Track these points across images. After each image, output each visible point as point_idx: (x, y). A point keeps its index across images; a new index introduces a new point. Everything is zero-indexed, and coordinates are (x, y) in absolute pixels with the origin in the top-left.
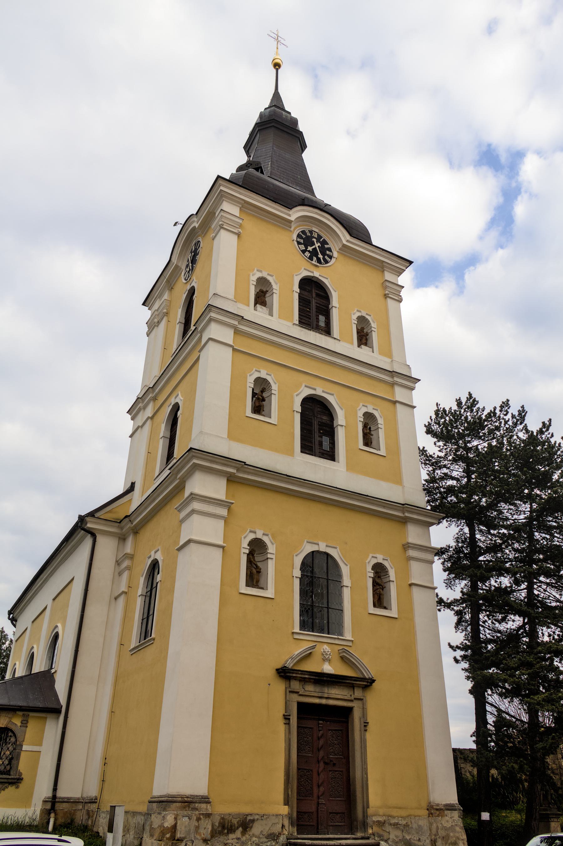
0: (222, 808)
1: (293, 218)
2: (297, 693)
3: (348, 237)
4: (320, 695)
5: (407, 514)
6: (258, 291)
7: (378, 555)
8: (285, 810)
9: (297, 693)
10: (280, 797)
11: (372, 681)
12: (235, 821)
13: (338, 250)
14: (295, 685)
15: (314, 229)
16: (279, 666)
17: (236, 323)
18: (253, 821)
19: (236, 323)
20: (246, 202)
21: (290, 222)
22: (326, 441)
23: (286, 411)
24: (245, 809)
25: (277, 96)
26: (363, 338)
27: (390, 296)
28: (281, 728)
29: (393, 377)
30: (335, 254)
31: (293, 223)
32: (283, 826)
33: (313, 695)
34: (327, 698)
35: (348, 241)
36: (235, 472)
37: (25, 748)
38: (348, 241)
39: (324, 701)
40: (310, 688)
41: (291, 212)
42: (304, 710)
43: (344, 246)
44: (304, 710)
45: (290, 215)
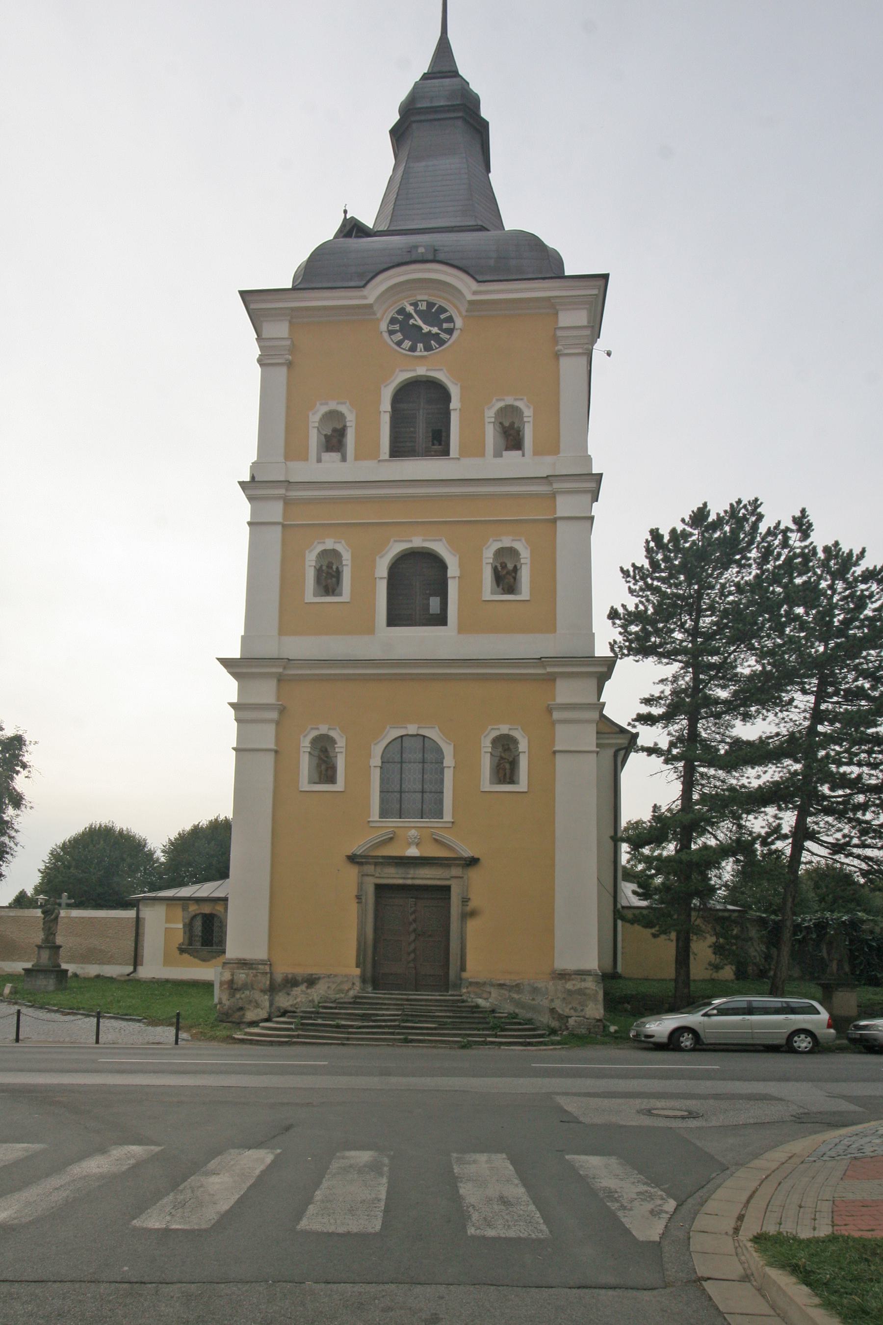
0: (282, 970)
1: (370, 300)
2: (373, 875)
3: (474, 286)
4: (403, 876)
5: (549, 670)
6: (329, 432)
7: (501, 726)
8: (358, 971)
9: (373, 875)
10: (353, 962)
11: (478, 859)
12: (300, 979)
13: (464, 313)
14: (370, 869)
15: (419, 298)
16: (349, 854)
17: (282, 491)
18: (319, 979)
19: (282, 491)
20: (293, 309)
21: (370, 306)
22: (434, 603)
23: (369, 582)
24: (310, 971)
25: (444, 49)
26: (512, 439)
27: (566, 351)
28: (354, 907)
29: (551, 484)
30: (459, 323)
31: (375, 308)
32: (353, 984)
33: (393, 876)
34: (413, 878)
35: (475, 293)
36: (281, 670)
37: (181, 926)
38: (475, 293)
39: (409, 882)
40: (391, 871)
41: (365, 291)
42: (381, 889)
43: (471, 303)
44: (381, 889)
45: (365, 297)
